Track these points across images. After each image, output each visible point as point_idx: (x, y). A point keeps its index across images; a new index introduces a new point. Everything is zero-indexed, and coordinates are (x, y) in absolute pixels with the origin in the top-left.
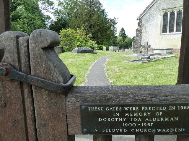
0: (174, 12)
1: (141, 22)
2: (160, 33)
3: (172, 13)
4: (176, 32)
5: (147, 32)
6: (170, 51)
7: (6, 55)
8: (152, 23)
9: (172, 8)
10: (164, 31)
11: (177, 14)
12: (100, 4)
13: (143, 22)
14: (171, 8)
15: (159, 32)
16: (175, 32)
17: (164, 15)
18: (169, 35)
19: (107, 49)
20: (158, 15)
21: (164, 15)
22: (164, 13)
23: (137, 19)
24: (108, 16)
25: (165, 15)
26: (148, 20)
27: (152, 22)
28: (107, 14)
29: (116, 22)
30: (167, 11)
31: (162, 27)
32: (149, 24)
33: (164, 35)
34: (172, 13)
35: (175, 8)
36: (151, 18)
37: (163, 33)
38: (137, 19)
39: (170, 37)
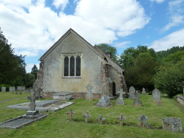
1: (43, 64)
2: (62, 76)
3: (72, 58)
5: (49, 75)
6: (70, 96)
8: (54, 65)
10: (66, 74)
11: (77, 59)
12: (5, 39)
13: (45, 63)
15: (61, 75)
16: (75, 76)
17: (65, 59)
18: (76, 78)
19: (7, 90)
20: (60, 58)
22: (65, 57)
23: (39, 60)
24: (14, 52)
25: (66, 59)
26: (50, 62)
28: (12, 50)
29: (23, 60)
30: (68, 55)
31: (63, 70)
32: (51, 66)
33: (65, 78)
34: (72, 58)
35: (74, 53)
36: (53, 60)
37: (64, 76)
38: (39, 60)
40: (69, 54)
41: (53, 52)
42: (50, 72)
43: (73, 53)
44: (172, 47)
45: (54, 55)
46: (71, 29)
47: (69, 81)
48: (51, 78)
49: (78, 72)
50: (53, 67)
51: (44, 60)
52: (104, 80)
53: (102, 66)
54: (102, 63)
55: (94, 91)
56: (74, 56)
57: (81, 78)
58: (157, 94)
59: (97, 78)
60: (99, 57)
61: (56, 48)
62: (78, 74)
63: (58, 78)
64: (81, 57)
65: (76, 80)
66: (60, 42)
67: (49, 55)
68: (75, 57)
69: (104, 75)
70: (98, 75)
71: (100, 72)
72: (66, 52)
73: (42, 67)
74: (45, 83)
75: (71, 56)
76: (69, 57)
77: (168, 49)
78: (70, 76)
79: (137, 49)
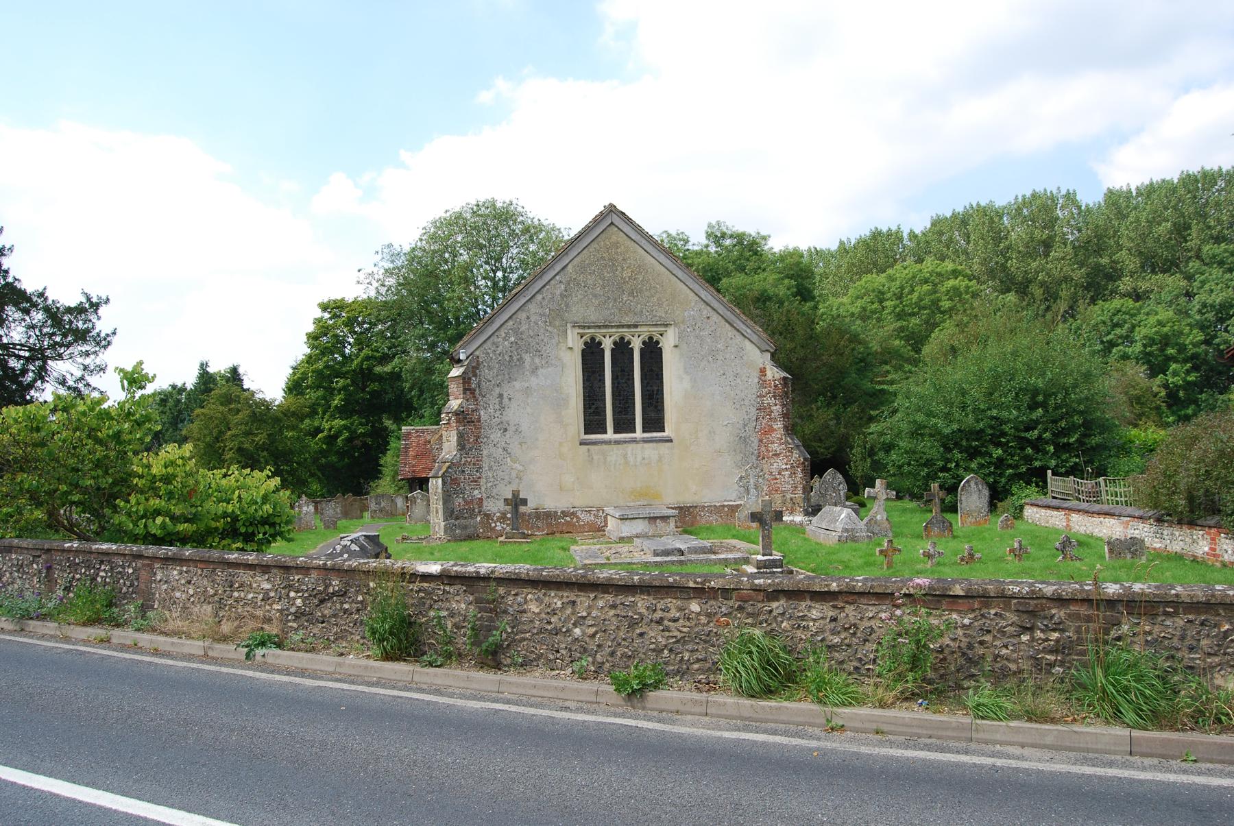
0: (600, 343)
3: (622, 348)
4: (644, 432)
5: (512, 429)
7: (524, 507)
8: (534, 381)
9: (623, 326)
10: (594, 423)
11: (642, 351)
13: (485, 372)
14: (618, 327)
16: (610, 435)
18: (645, 441)
21: (584, 354)
22: (586, 343)
25: (591, 353)
27: (533, 379)
30: (598, 334)
32: (517, 385)
34: (622, 348)
36: (527, 358)
39: (625, 456)
40: (606, 327)
41: (522, 315)
42: (512, 415)
43: (629, 326)
44: (865, 232)
45: (532, 333)
46: (611, 210)
47: (614, 453)
48: (521, 444)
49: (653, 415)
50: (527, 391)
51: (477, 353)
52: (776, 447)
53: (763, 386)
54: (763, 371)
55: (734, 495)
56: (599, 338)
57: (671, 441)
58: (975, 496)
59: (744, 440)
60: (747, 343)
61: (539, 297)
62: (654, 422)
63: (561, 444)
64: (668, 343)
65: (651, 451)
66: (558, 268)
67: (502, 333)
68: (636, 345)
69: (779, 425)
70: (745, 425)
71: (754, 412)
72: (593, 316)
73: (473, 392)
74: (490, 468)
75: (616, 337)
76: (607, 345)
77: (842, 243)
78: (615, 432)
79: (707, 246)
